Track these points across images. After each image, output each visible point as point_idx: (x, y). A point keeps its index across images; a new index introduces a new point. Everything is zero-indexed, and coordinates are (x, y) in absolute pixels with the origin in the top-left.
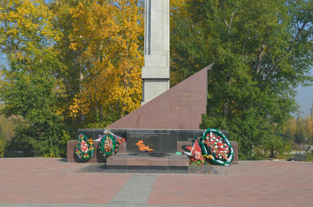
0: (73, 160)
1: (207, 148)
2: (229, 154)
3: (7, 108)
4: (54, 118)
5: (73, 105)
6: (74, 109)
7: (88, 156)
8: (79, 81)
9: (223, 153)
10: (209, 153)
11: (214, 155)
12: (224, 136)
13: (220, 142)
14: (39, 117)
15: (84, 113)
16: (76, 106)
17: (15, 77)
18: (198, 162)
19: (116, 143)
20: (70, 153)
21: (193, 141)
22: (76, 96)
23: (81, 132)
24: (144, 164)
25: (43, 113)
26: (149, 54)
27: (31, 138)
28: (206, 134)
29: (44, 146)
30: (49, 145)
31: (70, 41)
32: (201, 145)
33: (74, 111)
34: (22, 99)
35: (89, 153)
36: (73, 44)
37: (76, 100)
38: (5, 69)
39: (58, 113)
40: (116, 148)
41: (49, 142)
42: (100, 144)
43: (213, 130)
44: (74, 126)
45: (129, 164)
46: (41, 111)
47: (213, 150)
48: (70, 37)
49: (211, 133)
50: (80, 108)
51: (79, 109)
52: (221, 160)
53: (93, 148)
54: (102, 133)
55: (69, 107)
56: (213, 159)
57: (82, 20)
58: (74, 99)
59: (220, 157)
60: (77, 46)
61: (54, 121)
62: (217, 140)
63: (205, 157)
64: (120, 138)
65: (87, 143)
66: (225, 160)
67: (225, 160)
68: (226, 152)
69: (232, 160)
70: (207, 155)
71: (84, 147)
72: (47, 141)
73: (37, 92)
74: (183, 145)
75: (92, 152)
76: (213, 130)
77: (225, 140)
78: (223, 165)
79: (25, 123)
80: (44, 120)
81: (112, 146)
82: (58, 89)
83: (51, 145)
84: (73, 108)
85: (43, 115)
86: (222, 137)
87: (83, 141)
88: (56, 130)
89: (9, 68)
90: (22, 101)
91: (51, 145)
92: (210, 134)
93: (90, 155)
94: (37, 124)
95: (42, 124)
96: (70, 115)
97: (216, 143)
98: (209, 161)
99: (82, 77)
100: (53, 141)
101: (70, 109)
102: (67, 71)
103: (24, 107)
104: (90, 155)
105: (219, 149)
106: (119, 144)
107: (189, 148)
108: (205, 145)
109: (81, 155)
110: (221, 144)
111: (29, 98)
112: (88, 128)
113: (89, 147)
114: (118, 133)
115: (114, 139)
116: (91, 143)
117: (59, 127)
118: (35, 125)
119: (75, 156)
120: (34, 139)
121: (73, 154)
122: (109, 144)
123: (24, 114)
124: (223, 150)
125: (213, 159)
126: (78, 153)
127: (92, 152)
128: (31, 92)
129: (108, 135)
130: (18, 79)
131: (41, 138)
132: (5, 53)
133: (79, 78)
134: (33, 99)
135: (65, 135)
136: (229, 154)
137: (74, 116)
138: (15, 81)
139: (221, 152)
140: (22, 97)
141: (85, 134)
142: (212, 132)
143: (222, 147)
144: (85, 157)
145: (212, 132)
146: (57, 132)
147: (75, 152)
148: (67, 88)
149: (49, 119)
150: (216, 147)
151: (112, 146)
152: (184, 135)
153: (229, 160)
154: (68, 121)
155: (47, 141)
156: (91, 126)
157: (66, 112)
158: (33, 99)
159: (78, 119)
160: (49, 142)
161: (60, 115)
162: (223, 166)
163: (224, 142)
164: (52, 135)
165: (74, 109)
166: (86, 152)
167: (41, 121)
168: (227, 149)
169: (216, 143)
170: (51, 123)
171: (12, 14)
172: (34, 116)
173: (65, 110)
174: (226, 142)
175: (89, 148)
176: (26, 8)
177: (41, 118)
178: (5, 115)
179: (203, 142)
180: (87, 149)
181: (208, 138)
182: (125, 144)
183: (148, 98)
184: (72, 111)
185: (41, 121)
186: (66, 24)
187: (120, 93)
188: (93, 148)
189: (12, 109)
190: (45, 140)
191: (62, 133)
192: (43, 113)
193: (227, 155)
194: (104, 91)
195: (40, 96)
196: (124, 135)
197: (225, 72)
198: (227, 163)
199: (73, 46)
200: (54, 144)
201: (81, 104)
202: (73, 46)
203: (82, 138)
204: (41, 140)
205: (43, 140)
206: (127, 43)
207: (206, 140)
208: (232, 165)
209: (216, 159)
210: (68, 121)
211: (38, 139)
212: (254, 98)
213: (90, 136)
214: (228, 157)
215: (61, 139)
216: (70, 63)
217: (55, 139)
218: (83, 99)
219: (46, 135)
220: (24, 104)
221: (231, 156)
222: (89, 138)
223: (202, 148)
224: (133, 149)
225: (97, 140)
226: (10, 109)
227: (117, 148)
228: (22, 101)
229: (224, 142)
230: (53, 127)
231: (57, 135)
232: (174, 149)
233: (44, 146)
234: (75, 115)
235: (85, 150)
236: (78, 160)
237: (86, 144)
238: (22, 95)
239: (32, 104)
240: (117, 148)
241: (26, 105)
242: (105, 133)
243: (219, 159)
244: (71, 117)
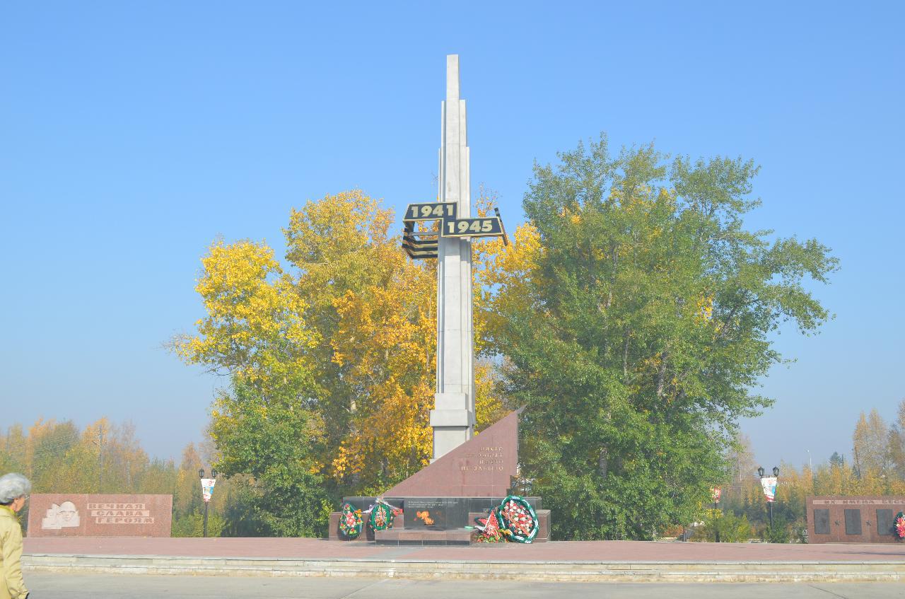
0: (337, 537)
1: (505, 521)
2: (532, 528)
3: (228, 462)
4: (307, 479)
5: (338, 458)
6: (340, 464)
7: (355, 532)
8: (350, 415)
9: (524, 528)
10: (507, 527)
11: (512, 530)
12: (529, 505)
13: (522, 513)
14: (283, 478)
15: (356, 471)
16: (343, 460)
17: (244, 411)
18: (492, 539)
19: (390, 515)
20: (332, 529)
21: (489, 512)
22: (343, 442)
23: (347, 501)
24: (419, 538)
25: (289, 470)
26: (443, 392)
27: (268, 513)
28: (505, 503)
29: (290, 527)
30: (298, 526)
31: (334, 349)
32: (498, 517)
33: (339, 468)
34: (256, 448)
35: (357, 528)
36: (338, 355)
37: (343, 450)
38: (227, 399)
39: (314, 470)
40: (390, 521)
41: (298, 521)
42: (370, 516)
43: (514, 497)
44: (339, 490)
45: (401, 538)
46: (286, 468)
47: (512, 523)
48: (333, 342)
49: (512, 502)
50: (350, 462)
51: (348, 465)
52: (521, 535)
53: (362, 522)
54: (373, 502)
55: (332, 461)
56: (511, 534)
57: (354, 317)
58: (340, 448)
59: (520, 532)
60: (344, 358)
61: (308, 486)
62: (519, 510)
63: (501, 532)
64: (396, 508)
65: (355, 516)
66: (525, 536)
67: (525, 536)
68: (528, 525)
69: (535, 536)
70: (505, 530)
71: (351, 520)
72: (294, 519)
73: (280, 435)
74: (476, 517)
75: (361, 527)
76: (514, 497)
77: (528, 510)
78: (523, 542)
79: (254, 487)
80: (291, 483)
81: (385, 519)
82: (314, 426)
83: (302, 525)
84: (338, 463)
85: (289, 475)
86: (525, 506)
87: (349, 512)
88: (310, 499)
89: (233, 396)
90: (256, 451)
91: (302, 525)
92: (509, 502)
93: (358, 531)
94: (279, 490)
95: (287, 489)
96: (333, 474)
97: (517, 515)
98: (506, 537)
99: (354, 407)
100: (305, 518)
101: (333, 464)
102: (329, 399)
103: (257, 462)
104: (358, 531)
105: (520, 522)
106: (394, 516)
107: (483, 521)
108: (503, 517)
109: (346, 530)
110: (522, 516)
111: (266, 445)
112: (364, 495)
113: (357, 520)
114: (392, 503)
115: (388, 509)
116: (359, 516)
117: (316, 496)
118: (275, 492)
119: (340, 532)
120: (273, 516)
121: (336, 530)
122: (381, 516)
123: (257, 472)
124: (525, 523)
125: (511, 534)
126: (343, 527)
127: (361, 527)
128: (268, 435)
129: (382, 505)
130: (249, 414)
131: (284, 514)
132: (224, 365)
133: (349, 408)
134: (273, 448)
135: (326, 508)
136: (532, 528)
137: (339, 477)
138: (242, 417)
139: (522, 525)
140: (255, 444)
141: (352, 503)
142: (514, 500)
143: (523, 519)
144: (351, 532)
145: (514, 500)
146: (312, 504)
147: (339, 527)
148: (328, 424)
149: (299, 481)
150: (517, 519)
151: (385, 519)
152: (479, 505)
153: (531, 535)
154: (330, 484)
155: (294, 519)
156: (369, 493)
157: (326, 470)
158: (273, 448)
159: (348, 479)
160: (298, 521)
161: (316, 474)
162: (522, 544)
163: (527, 512)
164: (304, 508)
165: (340, 464)
166: (353, 526)
167: (286, 484)
168: (530, 522)
169: (517, 515)
170: (302, 488)
171: (240, 308)
172: (274, 476)
173: (325, 465)
174: (530, 513)
175: (356, 522)
176: (263, 297)
177: (285, 480)
178: (224, 474)
179: (500, 513)
180: (355, 523)
181: (507, 508)
182: (402, 517)
183: (439, 454)
184: (335, 467)
185: (286, 484)
186: (323, 319)
187: (416, 437)
188: (362, 522)
189: (237, 463)
190: (290, 517)
191: (320, 505)
192: (289, 470)
193: (529, 530)
194: (390, 434)
195: (285, 442)
196: (401, 504)
197: (590, 398)
198: (529, 540)
199: (338, 358)
200: (306, 523)
201: (351, 455)
202: (338, 358)
203: (349, 508)
204: (284, 517)
205: (287, 517)
206: (426, 352)
207: (504, 510)
208: (534, 544)
209: (515, 534)
210: (330, 484)
211: (279, 516)
212: (639, 443)
213: (357, 506)
214: (530, 532)
215: (318, 516)
216: (335, 391)
217: (308, 515)
218: (355, 448)
219: (293, 508)
220: (257, 456)
221: (534, 531)
222: (357, 508)
223: (499, 521)
224: (411, 520)
225: (367, 512)
226: (233, 465)
227: (392, 521)
228: (256, 451)
229: (527, 512)
230: (305, 494)
231: (312, 508)
232: (464, 522)
233: (290, 527)
234: (342, 475)
235: (352, 524)
236: (344, 537)
237: (353, 517)
238: (255, 441)
239: (272, 455)
240: (392, 521)
241: (262, 457)
242: (377, 502)
243: (518, 535)
244: (334, 478)
